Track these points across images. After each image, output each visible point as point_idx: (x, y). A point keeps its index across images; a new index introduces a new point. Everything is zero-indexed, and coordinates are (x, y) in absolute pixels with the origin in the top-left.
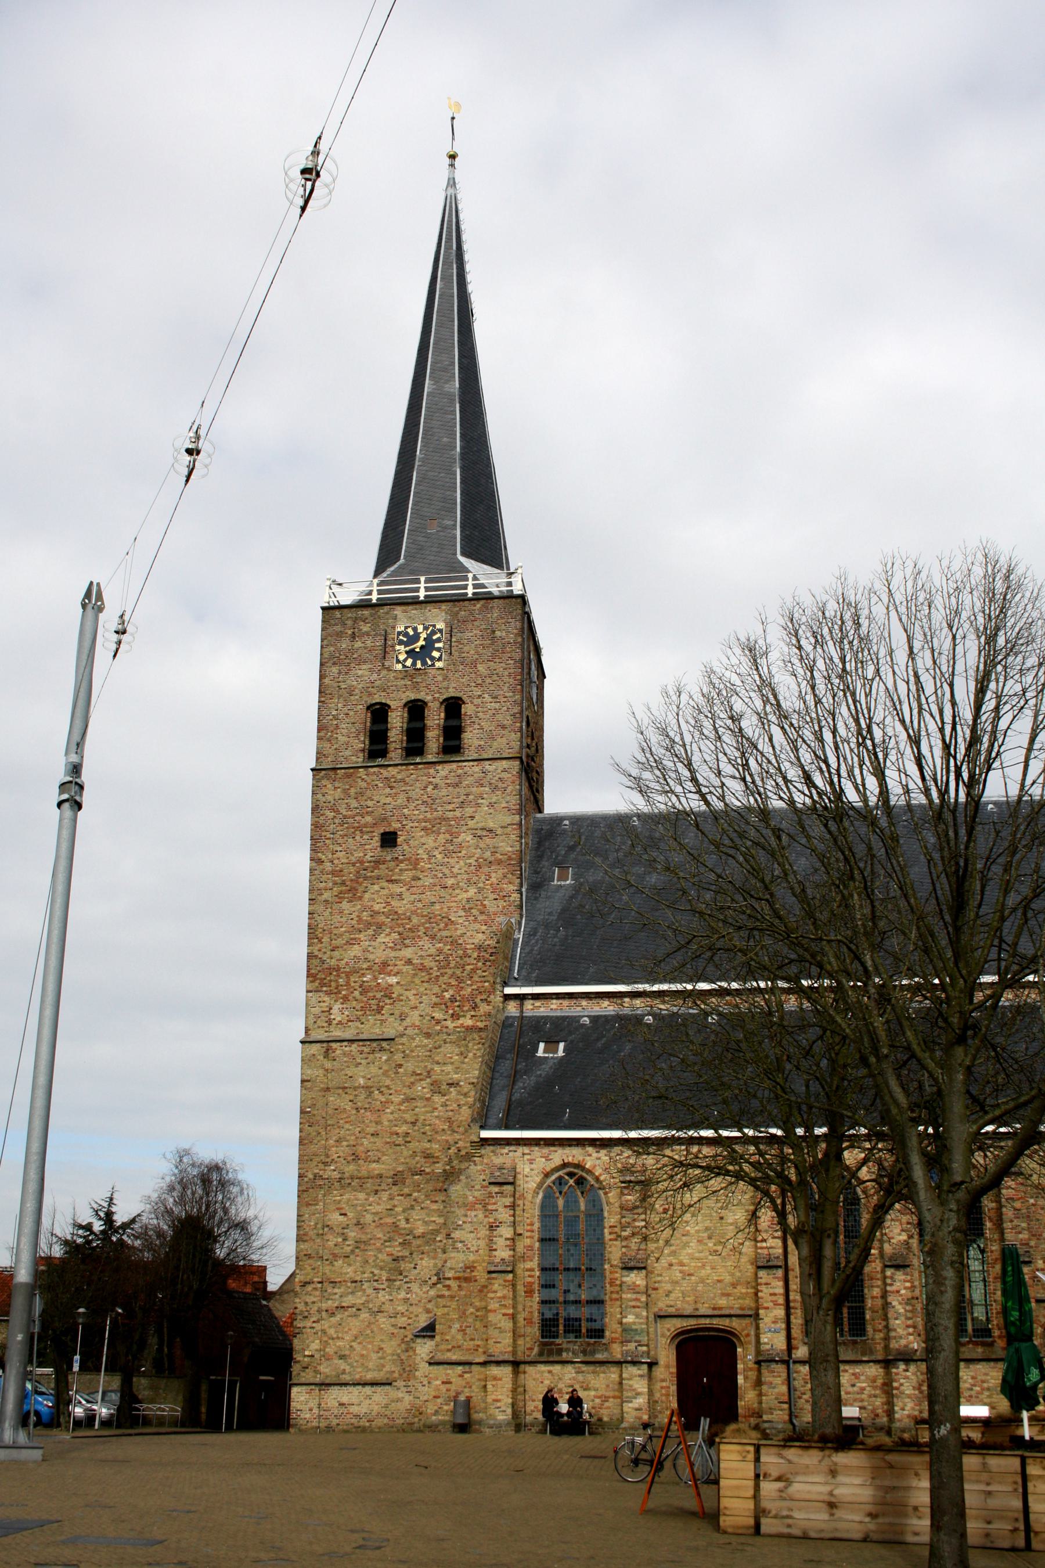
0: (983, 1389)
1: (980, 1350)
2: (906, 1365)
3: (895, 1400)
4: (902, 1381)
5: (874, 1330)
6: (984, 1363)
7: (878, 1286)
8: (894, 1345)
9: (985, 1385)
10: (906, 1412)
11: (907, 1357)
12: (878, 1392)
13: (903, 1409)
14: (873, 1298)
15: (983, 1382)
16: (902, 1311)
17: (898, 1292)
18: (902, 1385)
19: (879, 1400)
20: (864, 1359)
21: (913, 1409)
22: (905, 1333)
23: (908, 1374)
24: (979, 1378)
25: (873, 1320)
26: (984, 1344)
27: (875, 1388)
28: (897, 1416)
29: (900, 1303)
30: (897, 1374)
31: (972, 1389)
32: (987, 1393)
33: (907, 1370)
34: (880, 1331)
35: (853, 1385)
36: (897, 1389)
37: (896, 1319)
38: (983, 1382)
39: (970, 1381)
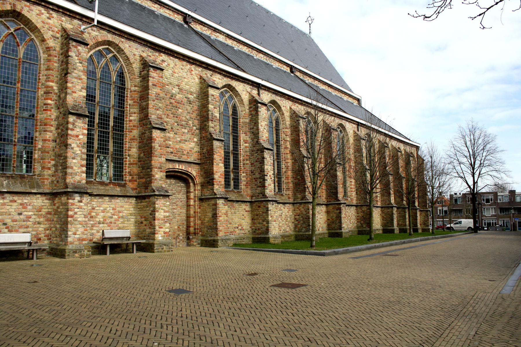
0: (119, 218)
1: (118, 189)
2: (81, 197)
3: (69, 226)
4: (76, 210)
5: (43, 168)
6: (121, 198)
7: (51, 132)
8: (69, 180)
9: (121, 214)
10: (77, 236)
11: (82, 191)
12: (42, 220)
13: (75, 234)
14: (44, 140)
15: (120, 212)
16: (79, 152)
17: (77, 136)
18: (76, 213)
19: (42, 226)
20: (33, 191)
21: (83, 233)
22: (79, 171)
23: (82, 204)
24: (117, 209)
25: (43, 159)
26: (120, 185)
27: (39, 216)
28: (70, 239)
29: (78, 146)
30: (73, 204)
31: (112, 218)
32: (121, 220)
33: (81, 201)
34: (49, 169)
35: (20, 214)
36: (72, 217)
37: (74, 158)
38: (120, 212)
39: (111, 211)
